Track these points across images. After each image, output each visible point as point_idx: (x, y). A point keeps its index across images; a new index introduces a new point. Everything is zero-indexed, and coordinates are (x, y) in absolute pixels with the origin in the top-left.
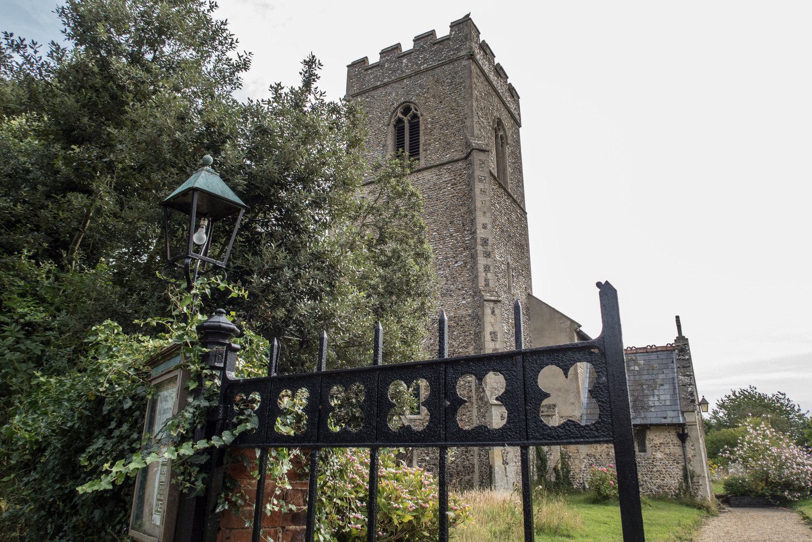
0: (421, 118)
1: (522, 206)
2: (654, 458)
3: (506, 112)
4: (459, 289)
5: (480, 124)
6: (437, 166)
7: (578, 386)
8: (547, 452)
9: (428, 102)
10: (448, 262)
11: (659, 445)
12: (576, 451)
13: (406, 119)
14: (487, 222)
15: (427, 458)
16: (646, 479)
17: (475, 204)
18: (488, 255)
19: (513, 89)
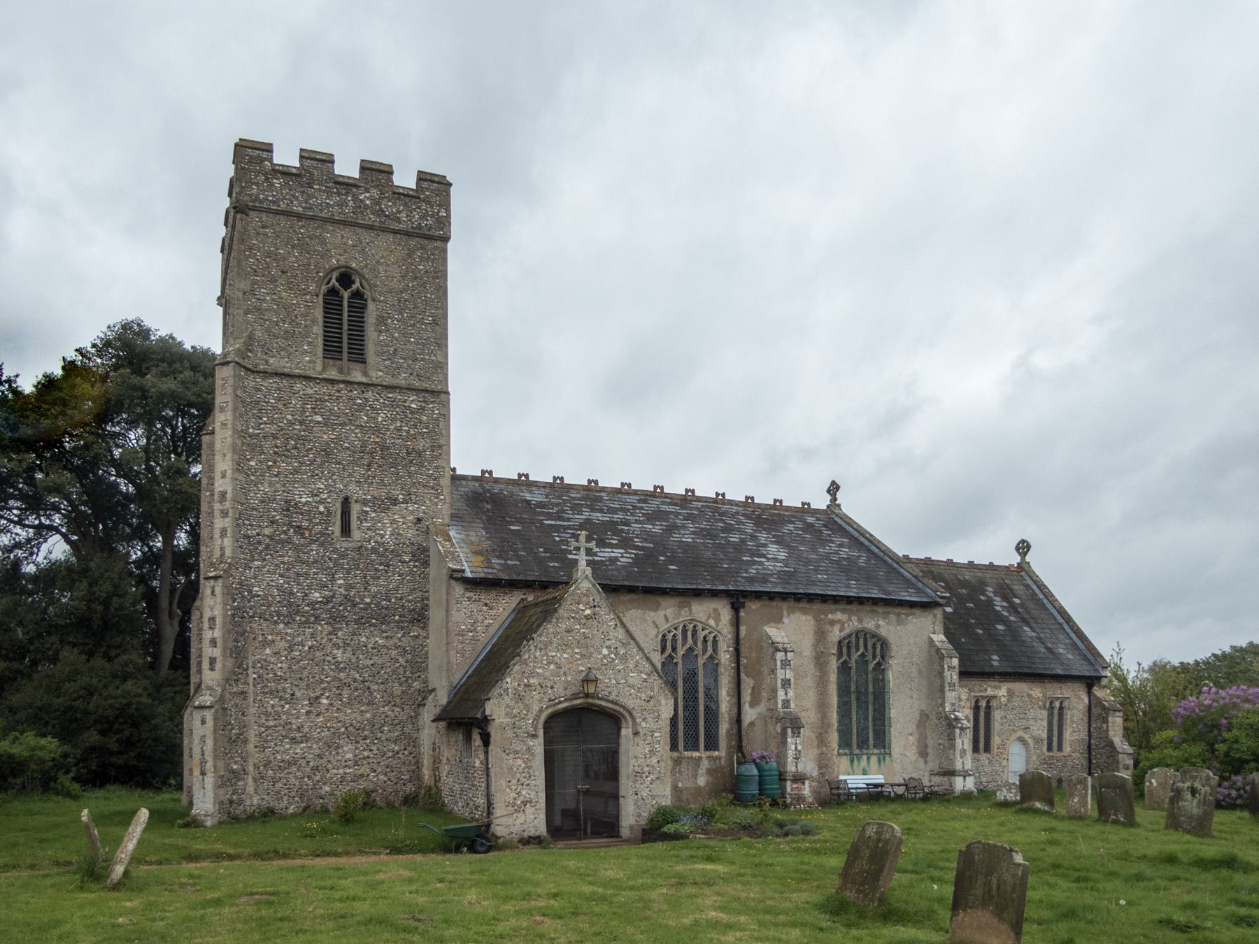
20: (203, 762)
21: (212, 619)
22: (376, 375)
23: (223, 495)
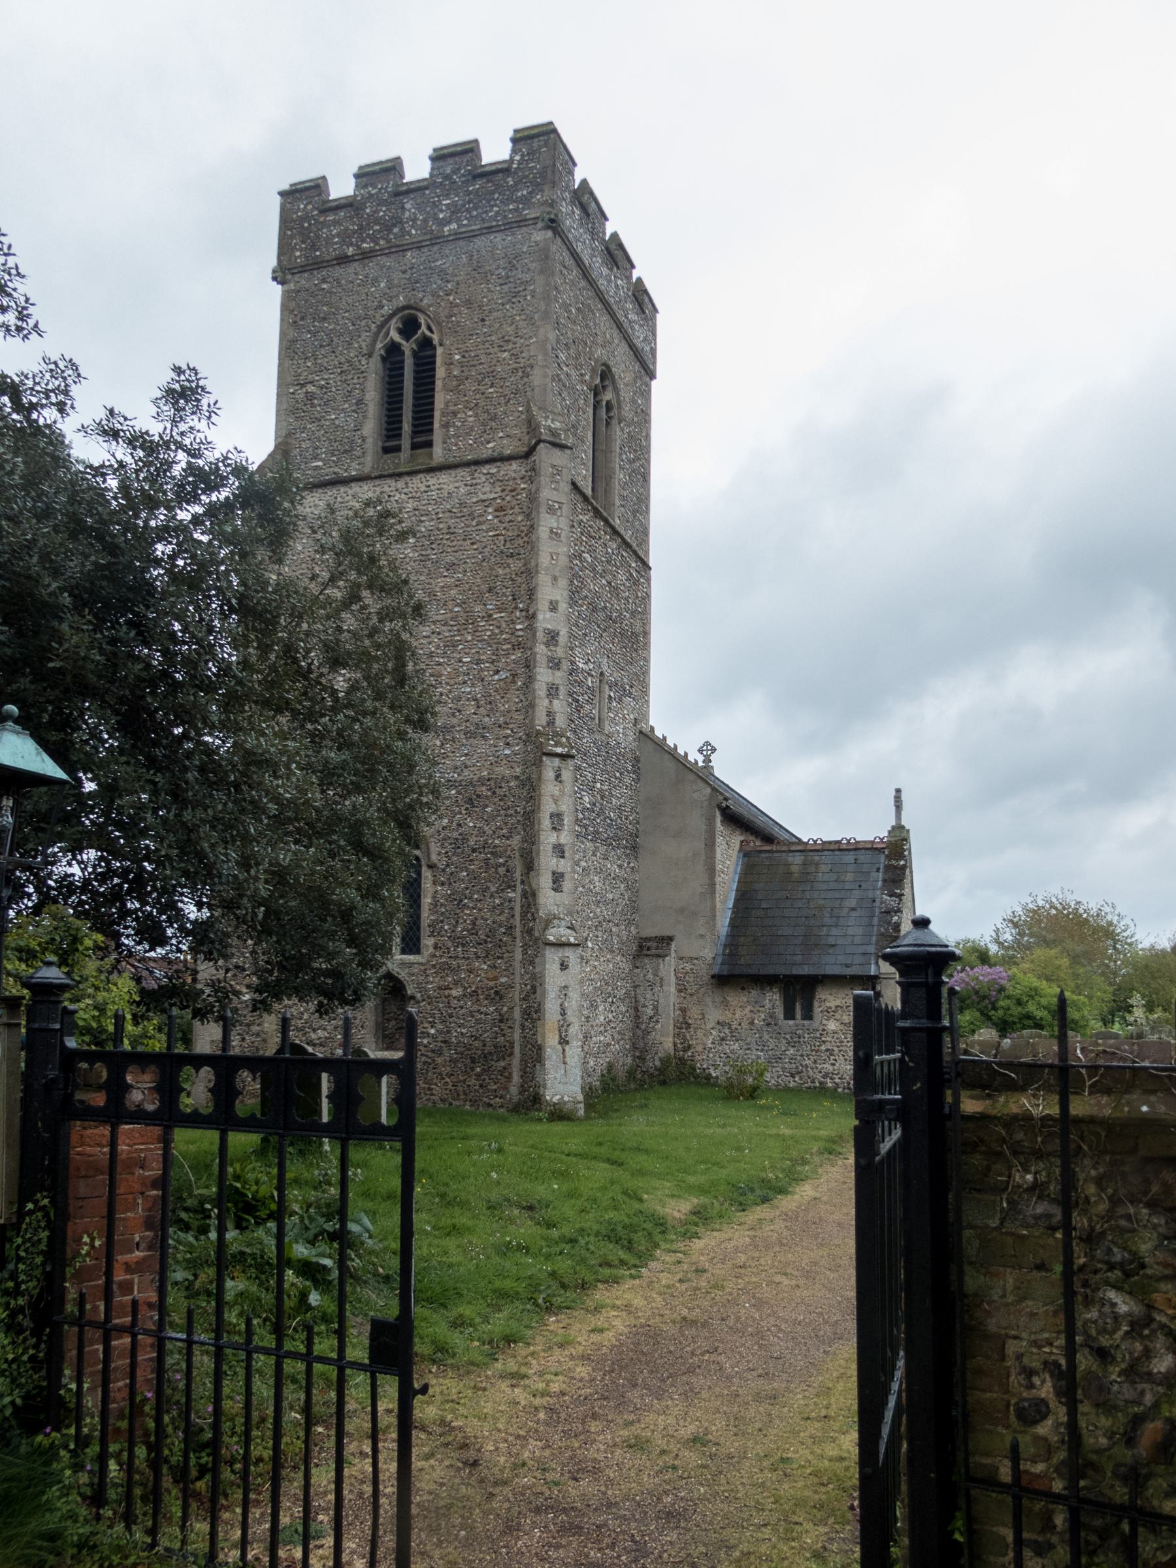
0: (439, 351)
1: (640, 553)
3: (623, 348)
4: (500, 726)
5: (560, 380)
6: (468, 464)
7: (713, 908)
8: (651, 1018)
9: (455, 315)
10: (482, 670)
13: (408, 347)
14: (558, 598)
15: (433, 1031)
16: (807, 1062)
17: (537, 559)
18: (555, 664)
19: (646, 292)
21: (557, 817)
23: (552, 637)
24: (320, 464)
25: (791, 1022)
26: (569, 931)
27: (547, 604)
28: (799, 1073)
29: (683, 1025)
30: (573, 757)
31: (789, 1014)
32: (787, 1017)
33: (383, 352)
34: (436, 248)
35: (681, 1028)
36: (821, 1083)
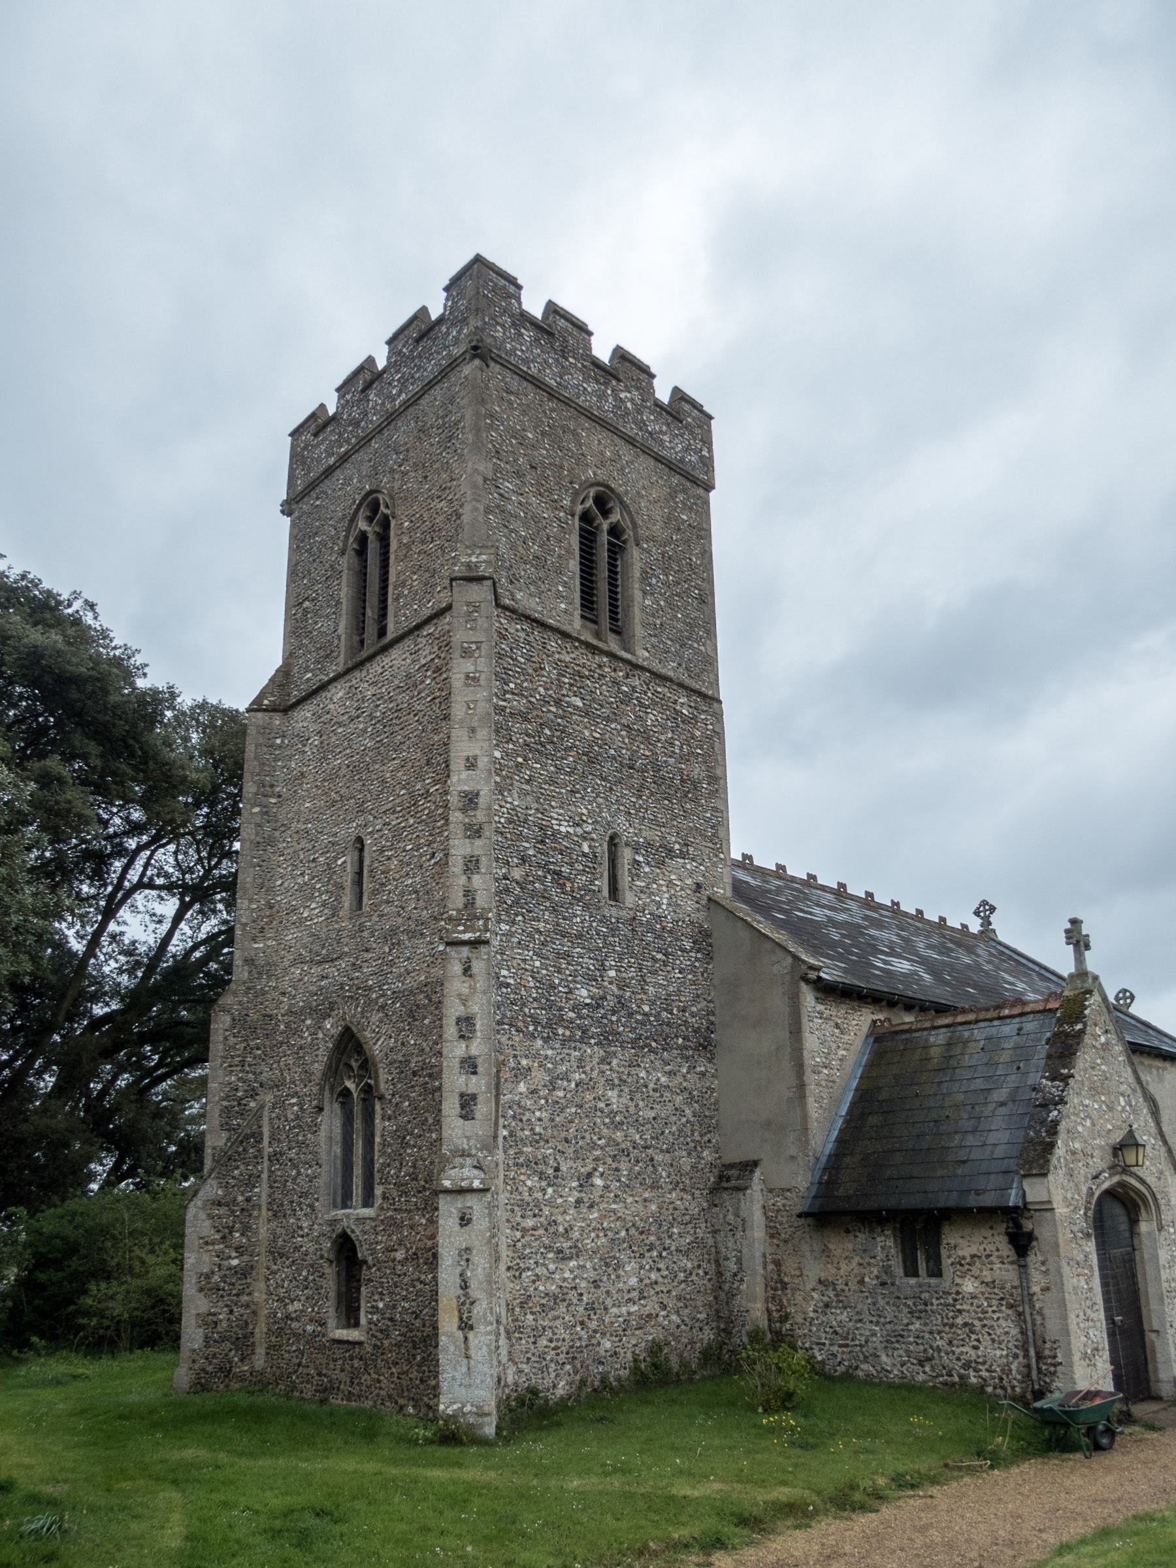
2: (958, 1293)
7: (805, 1117)
11: (968, 1260)
12: (798, 1273)
14: (478, 752)
16: (940, 1343)
20: (466, 1303)
21: (466, 1024)
22: (642, 655)
23: (470, 800)
24: (309, 675)
25: (913, 1281)
26: (476, 1172)
27: (462, 763)
28: (929, 1359)
29: (778, 1285)
30: (487, 942)
31: (911, 1270)
32: (907, 1274)
33: (355, 546)
34: (391, 427)
35: (775, 1289)
36: (961, 1377)
